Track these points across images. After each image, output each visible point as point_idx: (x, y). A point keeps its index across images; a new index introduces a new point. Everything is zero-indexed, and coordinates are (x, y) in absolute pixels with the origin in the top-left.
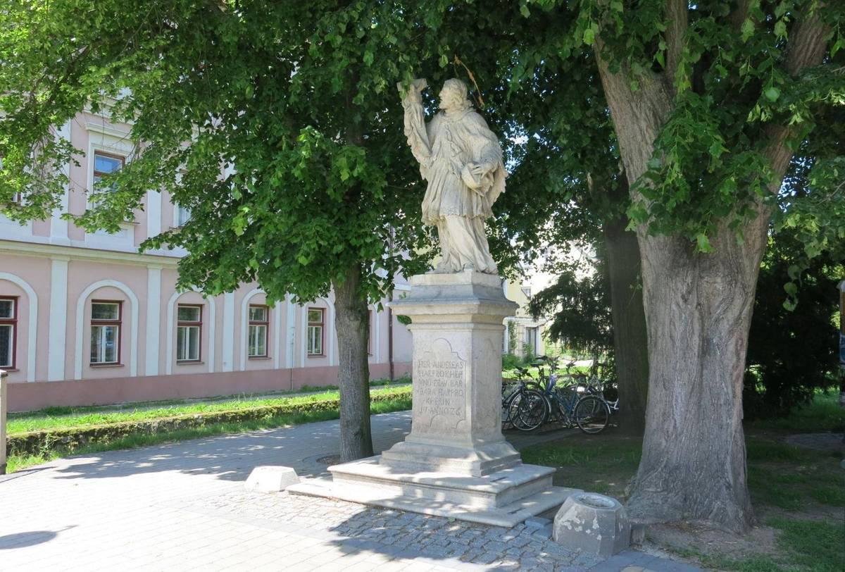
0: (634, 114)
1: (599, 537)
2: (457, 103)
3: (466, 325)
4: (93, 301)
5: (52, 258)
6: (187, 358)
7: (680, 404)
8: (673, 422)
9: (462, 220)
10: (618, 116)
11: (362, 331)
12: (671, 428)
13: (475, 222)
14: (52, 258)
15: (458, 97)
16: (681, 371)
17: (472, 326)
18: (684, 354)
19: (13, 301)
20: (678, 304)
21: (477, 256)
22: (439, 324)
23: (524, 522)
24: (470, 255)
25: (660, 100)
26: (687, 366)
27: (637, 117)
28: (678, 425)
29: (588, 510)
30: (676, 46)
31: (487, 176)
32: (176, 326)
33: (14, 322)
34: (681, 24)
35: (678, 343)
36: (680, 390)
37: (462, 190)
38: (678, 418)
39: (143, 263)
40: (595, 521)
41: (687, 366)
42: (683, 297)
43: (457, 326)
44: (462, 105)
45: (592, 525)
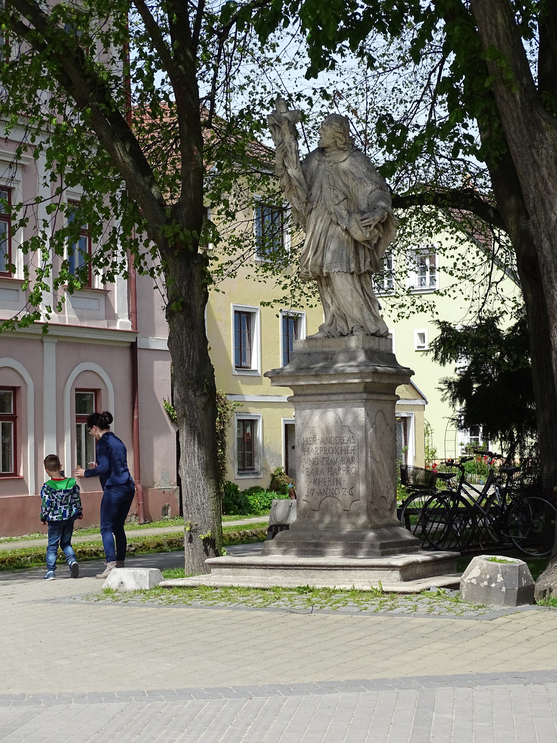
0: (535, 162)
1: (504, 589)
3: (358, 396)
15: (340, 136)
22: (327, 394)
23: (429, 589)
27: (538, 164)
29: (492, 565)
40: (499, 576)
43: (347, 396)
45: (497, 579)
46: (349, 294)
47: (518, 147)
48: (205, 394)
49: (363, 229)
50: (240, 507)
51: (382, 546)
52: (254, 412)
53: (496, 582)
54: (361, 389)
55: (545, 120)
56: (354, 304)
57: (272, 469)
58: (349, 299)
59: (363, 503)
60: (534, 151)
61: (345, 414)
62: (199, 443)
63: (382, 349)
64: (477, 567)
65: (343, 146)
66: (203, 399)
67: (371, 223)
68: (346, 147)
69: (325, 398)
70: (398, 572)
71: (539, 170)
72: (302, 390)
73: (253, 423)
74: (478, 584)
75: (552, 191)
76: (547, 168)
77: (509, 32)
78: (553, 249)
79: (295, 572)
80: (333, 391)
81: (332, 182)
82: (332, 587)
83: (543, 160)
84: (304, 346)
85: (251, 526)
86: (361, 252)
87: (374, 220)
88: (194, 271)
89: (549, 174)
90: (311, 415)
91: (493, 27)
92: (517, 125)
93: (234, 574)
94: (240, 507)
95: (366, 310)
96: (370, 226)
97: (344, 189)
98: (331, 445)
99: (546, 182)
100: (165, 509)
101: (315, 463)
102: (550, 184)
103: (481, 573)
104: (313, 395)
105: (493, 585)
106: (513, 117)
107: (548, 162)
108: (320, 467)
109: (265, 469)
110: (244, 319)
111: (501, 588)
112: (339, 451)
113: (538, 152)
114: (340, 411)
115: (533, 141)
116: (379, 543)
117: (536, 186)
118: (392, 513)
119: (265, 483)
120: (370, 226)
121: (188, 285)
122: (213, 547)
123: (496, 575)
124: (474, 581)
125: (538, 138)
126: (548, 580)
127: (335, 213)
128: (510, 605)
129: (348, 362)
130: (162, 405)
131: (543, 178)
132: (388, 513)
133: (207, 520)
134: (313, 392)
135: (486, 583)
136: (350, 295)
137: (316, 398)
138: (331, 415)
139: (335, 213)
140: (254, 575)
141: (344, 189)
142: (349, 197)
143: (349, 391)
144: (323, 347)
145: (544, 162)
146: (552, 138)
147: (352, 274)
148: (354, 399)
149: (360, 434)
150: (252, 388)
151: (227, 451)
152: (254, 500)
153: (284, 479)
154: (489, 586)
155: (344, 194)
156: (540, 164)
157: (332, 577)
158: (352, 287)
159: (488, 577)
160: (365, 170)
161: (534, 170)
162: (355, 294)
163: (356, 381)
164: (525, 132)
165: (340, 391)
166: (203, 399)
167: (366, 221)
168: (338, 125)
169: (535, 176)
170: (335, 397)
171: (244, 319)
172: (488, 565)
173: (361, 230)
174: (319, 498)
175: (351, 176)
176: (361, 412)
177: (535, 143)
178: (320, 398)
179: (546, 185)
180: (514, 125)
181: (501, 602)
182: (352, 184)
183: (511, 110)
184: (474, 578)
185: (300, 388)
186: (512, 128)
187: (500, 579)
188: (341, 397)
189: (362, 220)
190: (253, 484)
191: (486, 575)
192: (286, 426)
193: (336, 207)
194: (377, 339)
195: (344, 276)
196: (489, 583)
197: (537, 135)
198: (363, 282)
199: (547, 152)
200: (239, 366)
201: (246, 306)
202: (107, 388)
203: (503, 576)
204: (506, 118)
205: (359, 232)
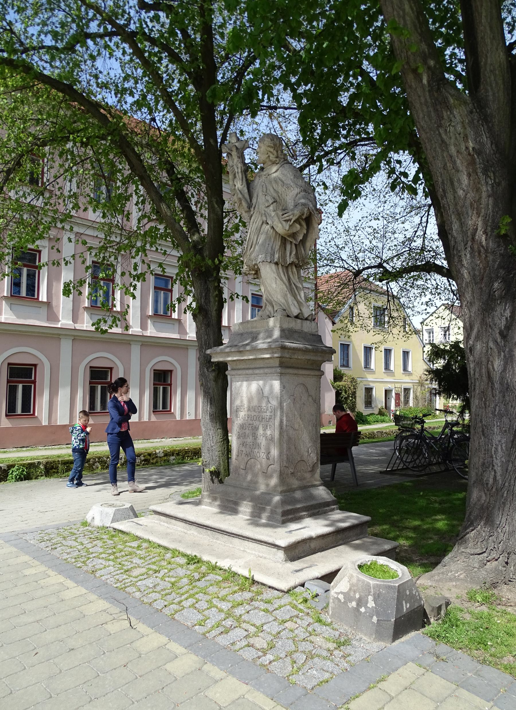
0: (443, 141)
1: (375, 619)
2: (271, 155)
3: (274, 370)
4: (91, 367)
5: (61, 337)
6: (161, 409)
7: (500, 453)
8: (493, 473)
9: (273, 266)
10: (429, 147)
11: (220, 381)
12: (491, 481)
13: (290, 270)
14: (61, 337)
15: (272, 150)
16: (501, 416)
17: (278, 370)
18: (504, 397)
19: (33, 367)
20: (495, 341)
21: (291, 303)
22: (252, 369)
23: (303, 585)
24: (283, 301)
25: (471, 122)
26: (506, 410)
27: (446, 143)
28: (498, 477)
29: (363, 581)
30: (489, 62)
31: (297, 221)
32: (152, 387)
33: (34, 382)
34: (494, 38)
35: (497, 386)
36: (499, 438)
37: (275, 238)
38: (498, 469)
39: (127, 340)
40: (370, 598)
41: (506, 410)
42: (501, 333)
43: (266, 370)
44: (277, 157)
45: (367, 602)
46: (274, 282)
47: (426, 133)
48: (214, 370)
49: (284, 223)
50: (363, 421)
51: (285, 513)
52: (372, 385)
53: (366, 607)
54: (277, 365)
55: (452, 96)
56: (278, 290)
57: (379, 407)
58: (274, 286)
59: (276, 467)
60: (442, 131)
61: (265, 385)
62: (211, 404)
63: (306, 331)
64: (346, 579)
65: (274, 159)
66: (214, 374)
67: (291, 217)
68: (277, 159)
69: (250, 371)
70: (283, 552)
71: (447, 148)
72: (236, 365)
73: (372, 389)
74: (345, 603)
75: (461, 168)
76: (455, 145)
77: (417, 22)
78: (462, 228)
79: (205, 531)
80: (258, 366)
81: (265, 190)
82: (213, 562)
83: (450, 138)
84: (239, 329)
85: (367, 430)
86: (288, 247)
87: (293, 214)
88: (210, 286)
89: (458, 152)
90: (241, 386)
91: (401, 19)
92: (425, 110)
93: (167, 523)
94: (363, 421)
95: (289, 296)
96: (290, 220)
97: (275, 195)
98: (255, 414)
99: (455, 160)
100: (330, 422)
101: (242, 427)
102: (458, 162)
103: (350, 589)
104: (244, 369)
105: (363, 610)
106: (421, 103)
107: (456, 138)
108: (247, 432)
109: (376, 407)
110: (368, 350)
111: (372, 617)
112: (260, 418)
113: (446, 130)
114: (261, 383)
115: (440, 121)
116: (281, 511)
117: (445, 167)
118: (313, 476)
119: (376, 411)
120: (290, 220)
121: (205, 296)
122: (218, 477)
123: (367, 596)
124: (341, 597)
125: (445, 117)
126: (452, 568)
127: (265, 214)
128: (383, 640)
129: (265, 339)
130: (329, 381)
131: (451, 157)
132: (308, 475)
133: (214, 458)
134: (243, 367)
135: (354, 604)
136: (274, 283)
137: (244, 372)
138: (254, 386)
139: (265, 214)
140: (179, 526)
141: (275, 195)
142: (278, 200)
143: (269, 365)
144: (252, 328)
145: (453, 140)
146: (460, 116)
147: (277, 264)
148: (271, 373)
149: (274, 403)
150: (371, 375)
151: (357, 398)
152: (370, 419)
153: (384, 410)
154: (357, 610)
155: (274, 198)
156: (448, 143)
157: (231, 543)
158: (275, 275)
159: (357, 596)
160: (292, 177)
161: (443, 151)
162: (279, 281)
163: (268, 356)
164: (433, 114)
165: (262, 366)
166: (214, 374)
167: (285, 215)
168: (269, 140)
169: (443, 157)
170: (257, 371)
171: (368, 350)
172: (359, 580)
173: (282, 224)
174: (246, 459)
175: (280, 183)
176: (276, 384)
177: (443, 122)
178: (247, 372)
179: (454, 163)
180: (423, 111)
181: (372, 635)
182: (280, 189)
183: (419, 97)
184: (341, 593)
185: (235, 363)
186: (421, 115)
187: (371, 604)
188: (262, 371)
189: (283, 215)
190: (371, 412)
191: (355, 592)
192: (386, 391)
193: (266, 209)
194: (299, 321)
195: (268, 266)
196: (358, 605)
197: (445, 114)
198: (290, 273)
199: (455, 129)
200: (366, 367)
201: (369, 345)
202: (176, 369)
203: (375, 600)
204: (415, 108)
205: (280, 225)
